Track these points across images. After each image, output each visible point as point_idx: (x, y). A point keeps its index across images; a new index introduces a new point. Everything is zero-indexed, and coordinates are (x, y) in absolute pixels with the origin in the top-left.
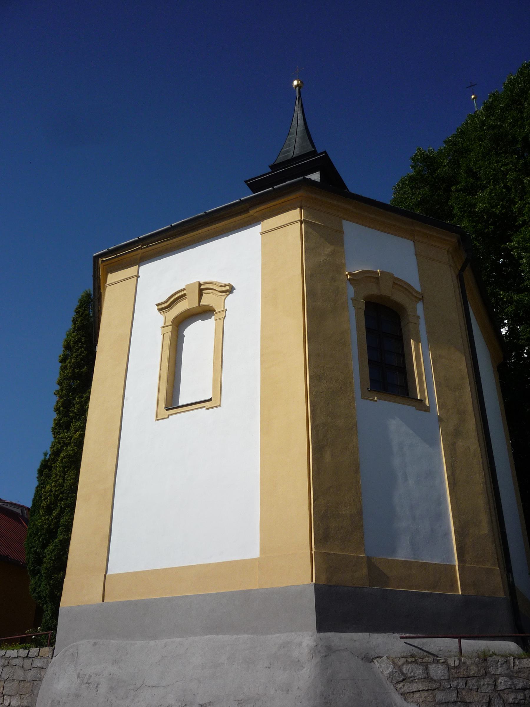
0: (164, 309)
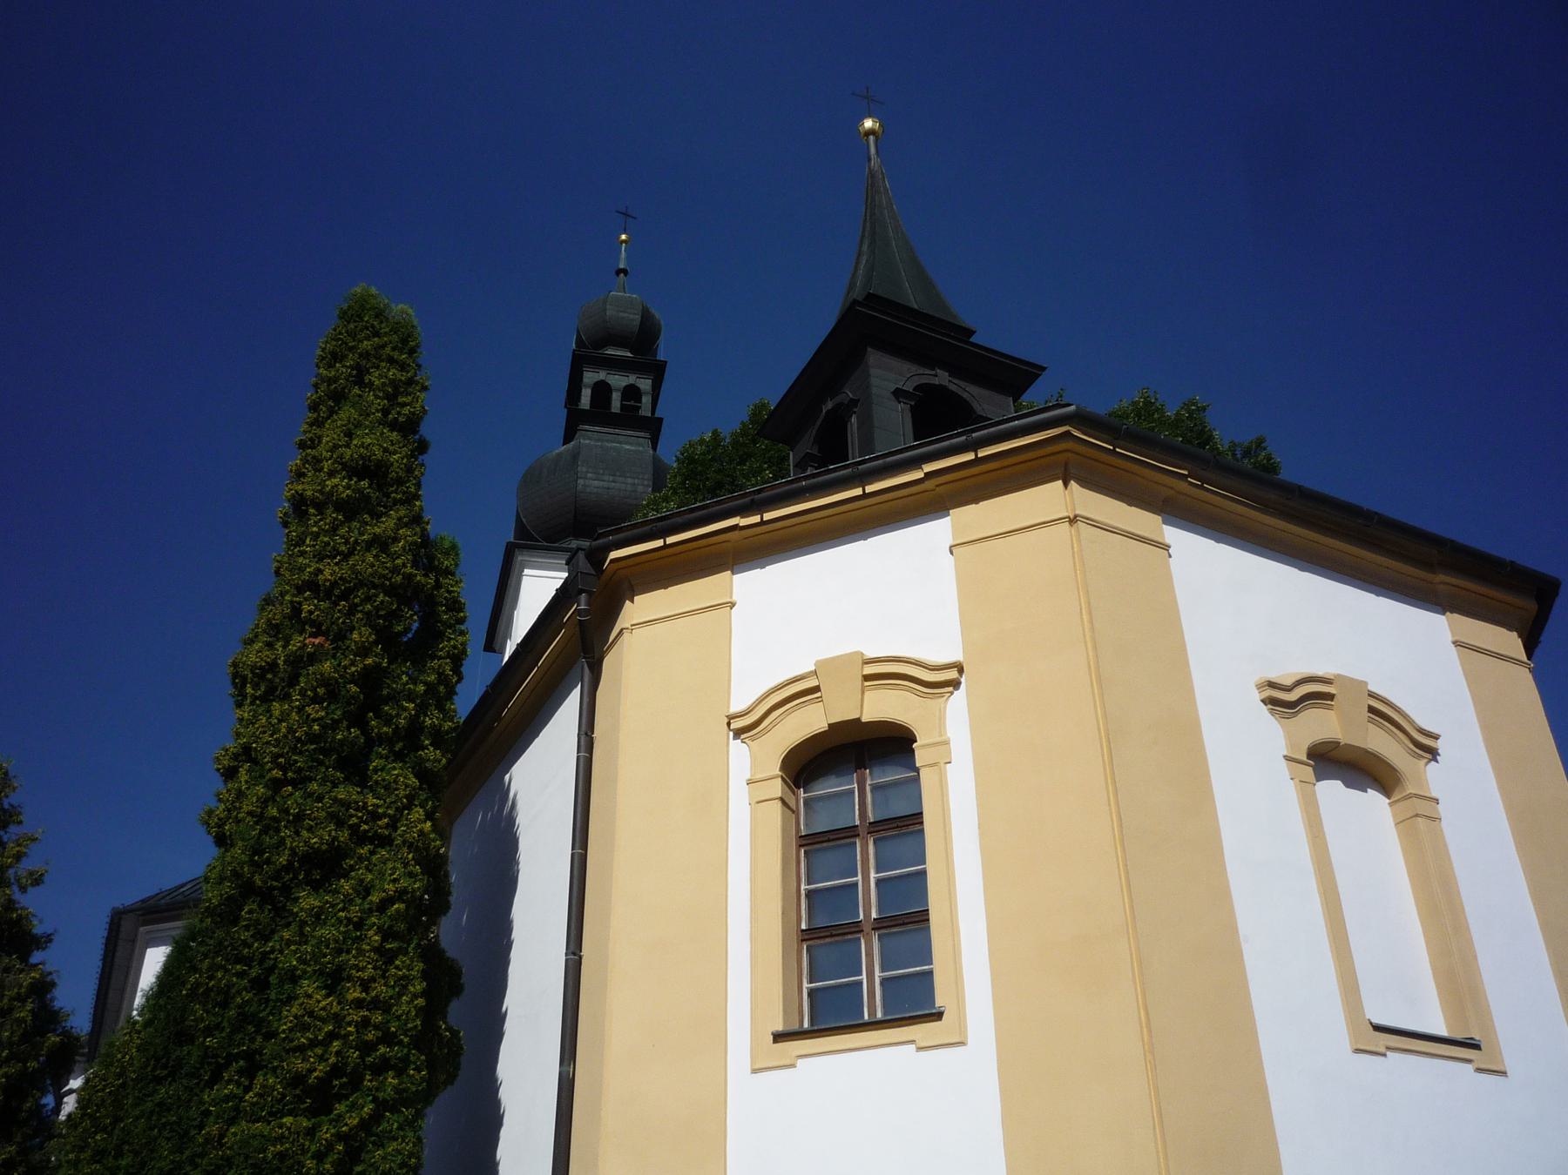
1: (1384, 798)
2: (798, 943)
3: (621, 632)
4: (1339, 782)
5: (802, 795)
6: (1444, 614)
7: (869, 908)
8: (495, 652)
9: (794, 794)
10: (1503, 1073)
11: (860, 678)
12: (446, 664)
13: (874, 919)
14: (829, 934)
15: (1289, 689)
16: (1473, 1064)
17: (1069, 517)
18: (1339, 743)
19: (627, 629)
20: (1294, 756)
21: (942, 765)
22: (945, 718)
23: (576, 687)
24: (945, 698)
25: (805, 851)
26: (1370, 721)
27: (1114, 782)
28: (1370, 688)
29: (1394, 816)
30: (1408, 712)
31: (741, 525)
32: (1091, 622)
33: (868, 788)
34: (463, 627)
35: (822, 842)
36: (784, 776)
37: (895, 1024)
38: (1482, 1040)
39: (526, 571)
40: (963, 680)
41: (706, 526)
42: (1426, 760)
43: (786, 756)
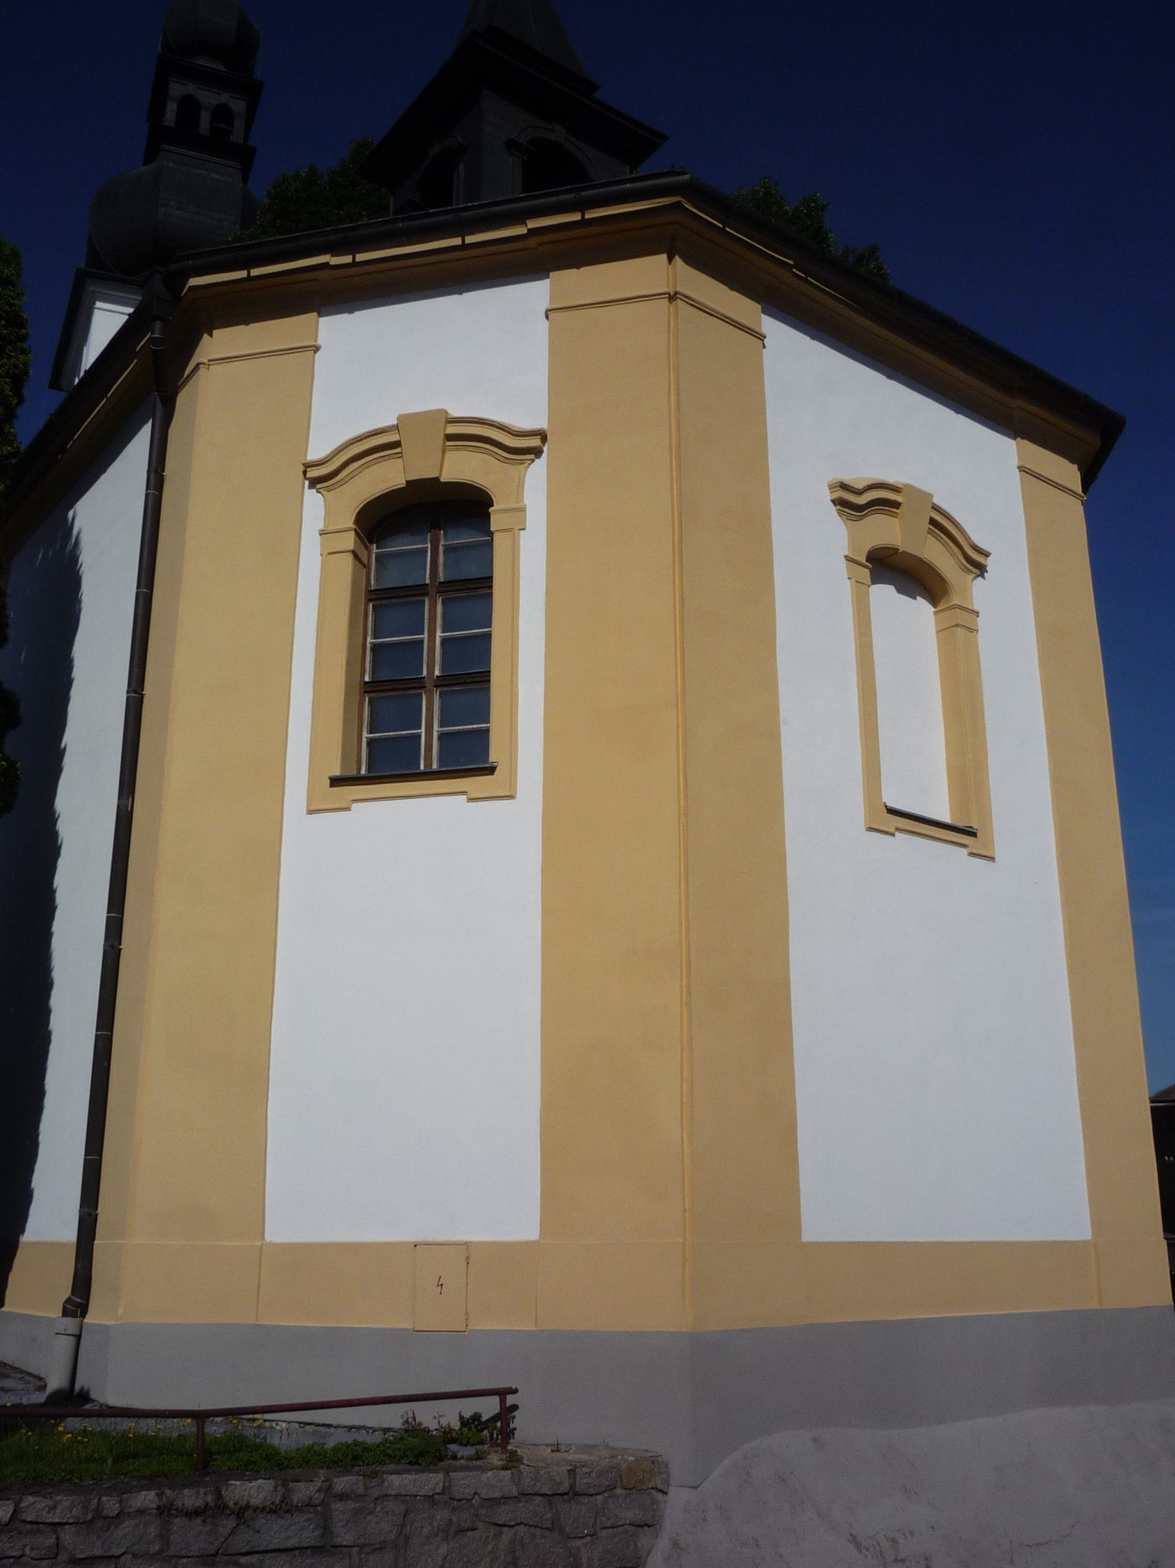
0: (852, 510)
1: (930, 606)
2: (360, 695)
3: (197, 368)
4: (892, 587)
5: (375, 551)
6: (1015, 439)
7: (434, 666)
8: (62, 391)
9: (367, 549)
10: (992, 859)
11: (442, 436)
12: (6, 383)
13: (437, 676)
14: (390, 687)
15: (859, 493)
16: (968, 849)
17: (669, 294)
18: (898, 550)
19: (204, 364)
20: (854, 557)
21: (516, 531)
22: (523, 486)
23: (147, 421)
24: (526, 465)
25: (374, 606)
26: (930, 532)
27: (681, 562)
28: (934, 501)
29: (937, 624)
30: (968, 532)
31: (331, 263)
32: (678, 403)
33: (441, 549)
34: (25, 346)
35: (392, 598)
36: (358, 529)
37: (450, 775)
38: (979, 829)
39: (99, 304)
40: (545, 449)
41: (292, 261)
42: (974, 575)
43: (361, 510)
